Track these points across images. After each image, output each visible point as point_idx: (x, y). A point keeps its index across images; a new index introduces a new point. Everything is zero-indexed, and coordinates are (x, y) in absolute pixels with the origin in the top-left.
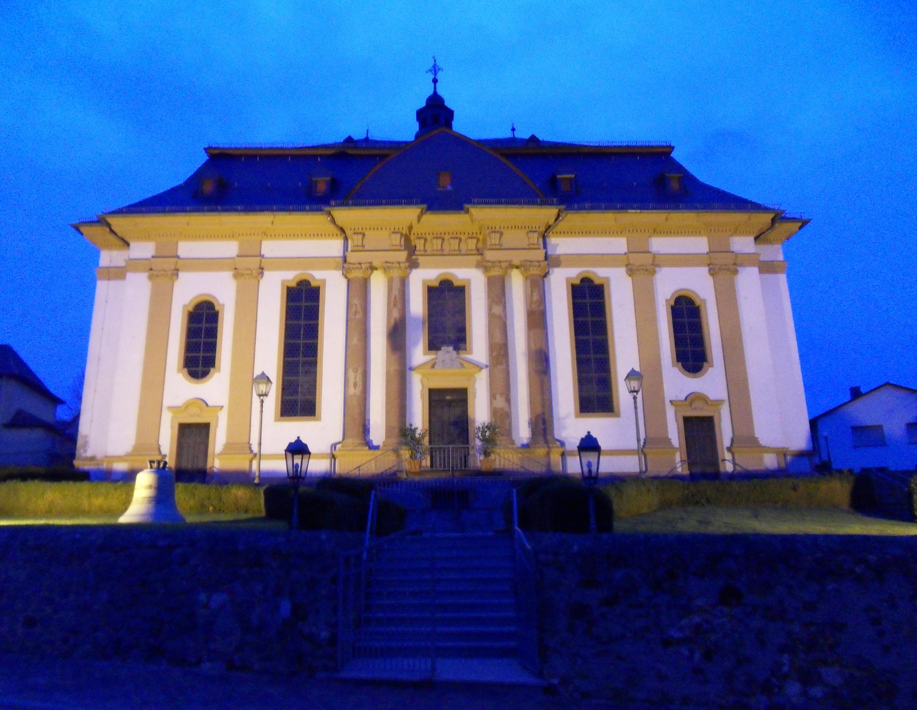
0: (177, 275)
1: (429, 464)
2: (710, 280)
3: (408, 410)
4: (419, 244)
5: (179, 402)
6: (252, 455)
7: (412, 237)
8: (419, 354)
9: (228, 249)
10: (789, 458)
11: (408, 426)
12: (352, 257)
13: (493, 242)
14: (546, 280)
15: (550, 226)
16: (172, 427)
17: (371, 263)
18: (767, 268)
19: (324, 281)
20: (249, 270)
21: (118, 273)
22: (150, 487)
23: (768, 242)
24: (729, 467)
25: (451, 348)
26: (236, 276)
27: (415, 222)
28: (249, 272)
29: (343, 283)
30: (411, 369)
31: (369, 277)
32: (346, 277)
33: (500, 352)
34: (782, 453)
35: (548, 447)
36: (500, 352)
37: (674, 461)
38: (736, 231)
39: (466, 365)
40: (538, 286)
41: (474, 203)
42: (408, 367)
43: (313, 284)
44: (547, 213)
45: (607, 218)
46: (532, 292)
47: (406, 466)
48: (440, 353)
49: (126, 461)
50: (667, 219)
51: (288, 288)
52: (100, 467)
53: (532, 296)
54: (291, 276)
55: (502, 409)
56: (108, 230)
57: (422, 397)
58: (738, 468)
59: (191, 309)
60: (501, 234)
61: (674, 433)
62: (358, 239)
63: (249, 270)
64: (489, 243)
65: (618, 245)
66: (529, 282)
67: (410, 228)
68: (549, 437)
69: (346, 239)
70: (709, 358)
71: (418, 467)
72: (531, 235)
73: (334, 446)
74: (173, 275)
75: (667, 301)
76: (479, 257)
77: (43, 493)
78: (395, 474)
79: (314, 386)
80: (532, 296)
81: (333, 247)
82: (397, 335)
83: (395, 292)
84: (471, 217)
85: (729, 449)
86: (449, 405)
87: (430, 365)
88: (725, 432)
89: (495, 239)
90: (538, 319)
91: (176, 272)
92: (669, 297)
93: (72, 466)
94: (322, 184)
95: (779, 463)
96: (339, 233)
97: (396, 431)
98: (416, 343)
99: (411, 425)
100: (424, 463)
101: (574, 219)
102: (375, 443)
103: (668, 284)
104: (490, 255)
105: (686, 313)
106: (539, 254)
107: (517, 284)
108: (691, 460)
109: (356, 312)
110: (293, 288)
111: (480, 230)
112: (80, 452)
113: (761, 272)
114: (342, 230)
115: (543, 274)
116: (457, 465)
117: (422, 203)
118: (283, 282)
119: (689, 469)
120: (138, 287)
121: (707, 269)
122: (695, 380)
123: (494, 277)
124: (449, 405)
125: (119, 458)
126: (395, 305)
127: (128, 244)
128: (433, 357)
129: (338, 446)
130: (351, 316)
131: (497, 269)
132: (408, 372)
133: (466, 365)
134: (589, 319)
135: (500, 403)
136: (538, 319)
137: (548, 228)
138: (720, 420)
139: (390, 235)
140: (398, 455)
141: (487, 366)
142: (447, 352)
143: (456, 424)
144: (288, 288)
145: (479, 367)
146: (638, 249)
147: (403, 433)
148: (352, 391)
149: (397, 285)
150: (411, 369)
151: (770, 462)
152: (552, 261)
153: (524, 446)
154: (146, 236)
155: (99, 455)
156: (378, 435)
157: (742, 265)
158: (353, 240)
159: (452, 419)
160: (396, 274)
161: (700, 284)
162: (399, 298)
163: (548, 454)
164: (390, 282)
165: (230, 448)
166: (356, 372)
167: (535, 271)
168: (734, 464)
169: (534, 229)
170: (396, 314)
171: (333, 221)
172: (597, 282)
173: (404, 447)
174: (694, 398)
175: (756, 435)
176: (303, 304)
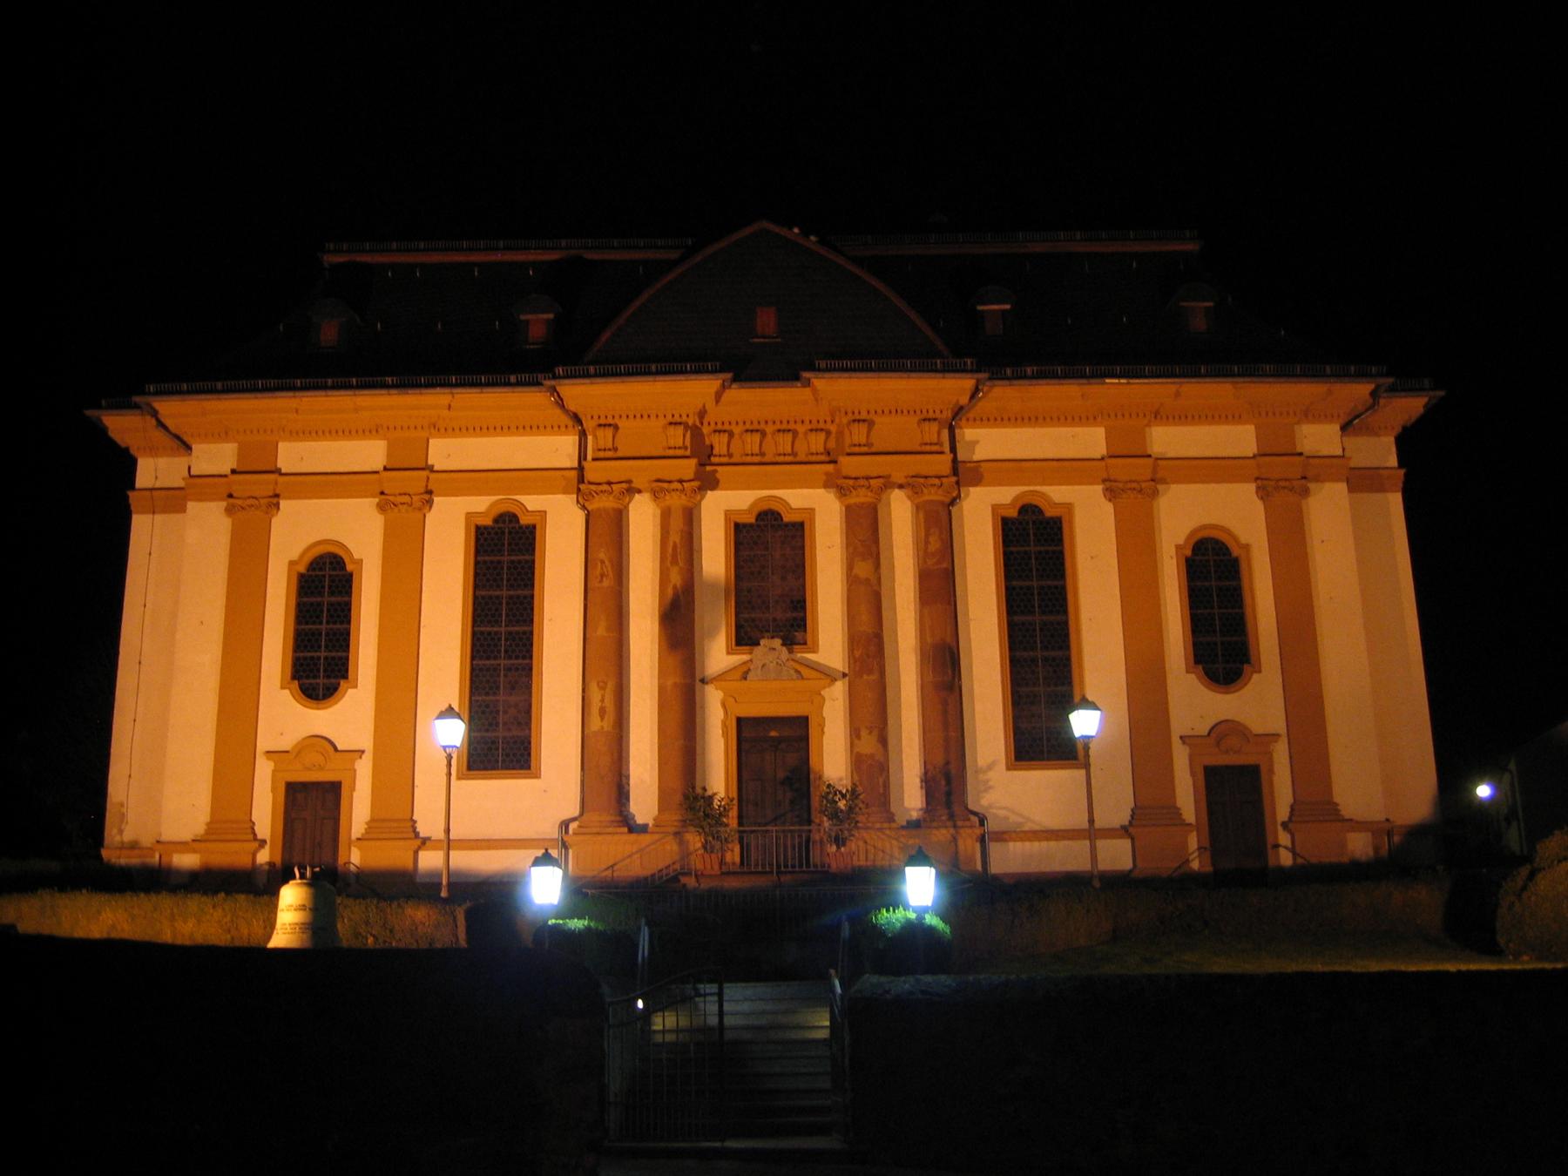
0: (277, 506)
1: (737, 859)
2: (1259, 506)
3: (698, 758)
4: (719, 444)
5: (286, 743)
6: (418, 842)
7: (706, 430)
8: (718, 654)
9: (370, 454)
10: (1396, 839)
11: (699, 790)
12: (594, 471)
13: (856, 439)
14: (954, 510)
15: (961, 408)
16: (274, 790)
17: (629, 482)
18: (1362, 481)
19: (543, 514)
20: (405, 491)
21: (172, 500)
22: (302, 908)
23: (1371, 431)
24: (1286, 859)
25: (777, 642)
26: (381, 508)
27: (710, 405)
28: (406, 499)
29: (580, 517)
30: (703, 681)
31: (626, 507)
32: (584, 507)
33: (869, 648)
34: (1382, 830)
35: (955, 826)
36: (869, 648)
37: (1185, 845)
38: (1309, 415)
39: (805, 672)
40: (939, 526)
41: (819, 370)
42: (698, 676)
43: (525, 520)
44: (956, 387)
45: (1068, 392)
46: (927, 536)
47: (697, 863)
48: (758, 651)
49: (195, 851)
50: (1177, 394)
51: (478, 528)
52: (148, 860)
53: (927, 542)
54: (482, 504)
55: (872, 756)
56: (154, 422)
57: (725, 734)
58: (1299, 860)
59: (302, 569)
60: (871, 424)
61: (1186, 797)
62: (606, 437)
63: (405, 491)
64: (848, 441)
65: (1091, 441)
66: (921, 515)
67: (702, 414)
68: (957, 809)
69: (583, 435)
70: (1253, 659)
71: (716, 867)
72: (926, 425)
73: (565, 825)
74: (269, 505)
75: (1178, 547)
76: (830, 467)
77: (99, 912)
78: (675, 879)
79: (528, 711)
80: (927, 542)
81: (560, 449)
82: (678, 619)
83: (675, 537)
84: (815, 391)
85: (1285, 825)
86: (774, 747)
87: (738, 674)
88: (1281, 794)
89: (859, 434)
90: (940, 585)
91: (273, 502)
92: (1181, 541)
93: (99, 857)
94: (537, 323)
95: (1376, 849)
96: (570, 423)
97: (678, 798)
98: (712, 633)
99: (704, 789)
100: (728, 857)
101: (1004, 394)
102: (640, 820)
103: (1181, 515)
104: (850, 465)
105: (1213, 570)
106: (942, 463)
107: (900, 514)
108: (1216, 843)
109: (602, 576)
110: (486, 528)
111: (833, 415)
112: (112, 835)
113: (1351, 490)
114: (577, 419)
115: (947, 500)
116: (771, 865)
117: (721, 371)
118: (469, 516)
119: (1213, 865)
120: (207, 527)
121: (1252, 487)
122: (1219, 697)
123: (860, 506)
124: (774, 747)
125: (183, 846)
126: (674, 561)
127: (189, 448)
128: (745, 657)
129: (573, 826)
130: (593, 583)
131: (862, 491)
132: (698, 685)
133: (805, 672)
134: (1035, 584)
135: (868, 745)
136: (940, 585)
137: (959, 411)
138: (1271, 771)
139: (665, 428)
140: (681, 843)
141: (844, 675)
142: (770, 649)
143: (787, 782)
144: (478, 528)
145: (830, 676)
146: (1127, 450)
147: (688, 799)
148: (596, 723)
149: (677, 523)
150: (703, 681)
151: (1359, 846)
152: (964, 474)
153: (914, 825)
154: (224, 435)
155: (146, 840)
156: (644, 802)
157: (1318, 479)
158: (595, 437)
159: (781, 775)
160: (676, 501)
161: (1239, 513)
162: (681, 546)
163: (955, 839)
164: (666, 515)
165: (378, 829)
166: (602, 688)
167: (933, 495)
168: (1295, 854)
169: (931, 415)
170: (676, 578)
171: (560, 403)
172: (1050, 512)
173: (692, 829)
174: (1225, 731)
175: (1337, 799)
176: (504, 561)
